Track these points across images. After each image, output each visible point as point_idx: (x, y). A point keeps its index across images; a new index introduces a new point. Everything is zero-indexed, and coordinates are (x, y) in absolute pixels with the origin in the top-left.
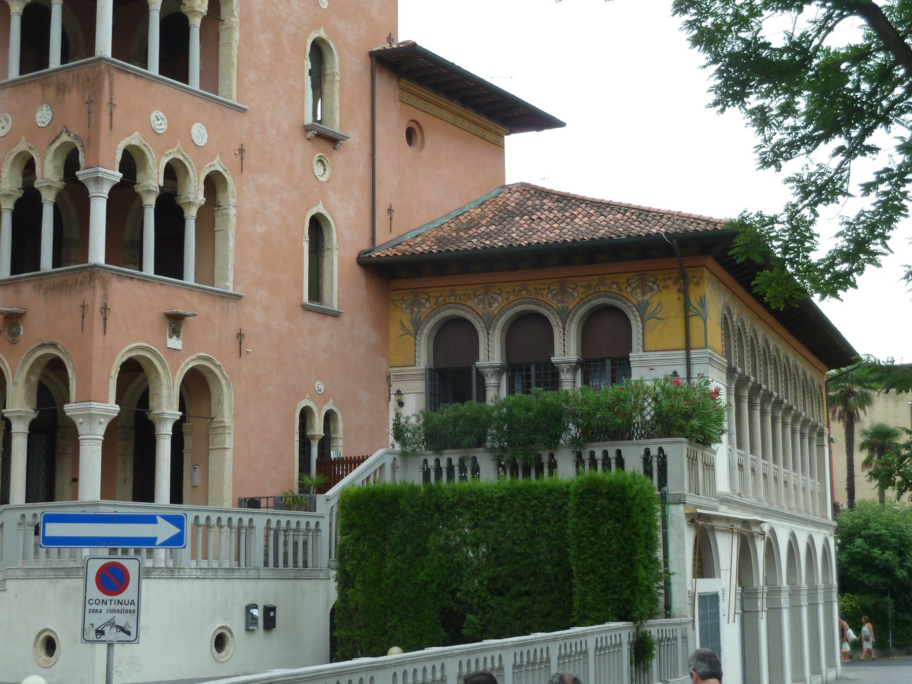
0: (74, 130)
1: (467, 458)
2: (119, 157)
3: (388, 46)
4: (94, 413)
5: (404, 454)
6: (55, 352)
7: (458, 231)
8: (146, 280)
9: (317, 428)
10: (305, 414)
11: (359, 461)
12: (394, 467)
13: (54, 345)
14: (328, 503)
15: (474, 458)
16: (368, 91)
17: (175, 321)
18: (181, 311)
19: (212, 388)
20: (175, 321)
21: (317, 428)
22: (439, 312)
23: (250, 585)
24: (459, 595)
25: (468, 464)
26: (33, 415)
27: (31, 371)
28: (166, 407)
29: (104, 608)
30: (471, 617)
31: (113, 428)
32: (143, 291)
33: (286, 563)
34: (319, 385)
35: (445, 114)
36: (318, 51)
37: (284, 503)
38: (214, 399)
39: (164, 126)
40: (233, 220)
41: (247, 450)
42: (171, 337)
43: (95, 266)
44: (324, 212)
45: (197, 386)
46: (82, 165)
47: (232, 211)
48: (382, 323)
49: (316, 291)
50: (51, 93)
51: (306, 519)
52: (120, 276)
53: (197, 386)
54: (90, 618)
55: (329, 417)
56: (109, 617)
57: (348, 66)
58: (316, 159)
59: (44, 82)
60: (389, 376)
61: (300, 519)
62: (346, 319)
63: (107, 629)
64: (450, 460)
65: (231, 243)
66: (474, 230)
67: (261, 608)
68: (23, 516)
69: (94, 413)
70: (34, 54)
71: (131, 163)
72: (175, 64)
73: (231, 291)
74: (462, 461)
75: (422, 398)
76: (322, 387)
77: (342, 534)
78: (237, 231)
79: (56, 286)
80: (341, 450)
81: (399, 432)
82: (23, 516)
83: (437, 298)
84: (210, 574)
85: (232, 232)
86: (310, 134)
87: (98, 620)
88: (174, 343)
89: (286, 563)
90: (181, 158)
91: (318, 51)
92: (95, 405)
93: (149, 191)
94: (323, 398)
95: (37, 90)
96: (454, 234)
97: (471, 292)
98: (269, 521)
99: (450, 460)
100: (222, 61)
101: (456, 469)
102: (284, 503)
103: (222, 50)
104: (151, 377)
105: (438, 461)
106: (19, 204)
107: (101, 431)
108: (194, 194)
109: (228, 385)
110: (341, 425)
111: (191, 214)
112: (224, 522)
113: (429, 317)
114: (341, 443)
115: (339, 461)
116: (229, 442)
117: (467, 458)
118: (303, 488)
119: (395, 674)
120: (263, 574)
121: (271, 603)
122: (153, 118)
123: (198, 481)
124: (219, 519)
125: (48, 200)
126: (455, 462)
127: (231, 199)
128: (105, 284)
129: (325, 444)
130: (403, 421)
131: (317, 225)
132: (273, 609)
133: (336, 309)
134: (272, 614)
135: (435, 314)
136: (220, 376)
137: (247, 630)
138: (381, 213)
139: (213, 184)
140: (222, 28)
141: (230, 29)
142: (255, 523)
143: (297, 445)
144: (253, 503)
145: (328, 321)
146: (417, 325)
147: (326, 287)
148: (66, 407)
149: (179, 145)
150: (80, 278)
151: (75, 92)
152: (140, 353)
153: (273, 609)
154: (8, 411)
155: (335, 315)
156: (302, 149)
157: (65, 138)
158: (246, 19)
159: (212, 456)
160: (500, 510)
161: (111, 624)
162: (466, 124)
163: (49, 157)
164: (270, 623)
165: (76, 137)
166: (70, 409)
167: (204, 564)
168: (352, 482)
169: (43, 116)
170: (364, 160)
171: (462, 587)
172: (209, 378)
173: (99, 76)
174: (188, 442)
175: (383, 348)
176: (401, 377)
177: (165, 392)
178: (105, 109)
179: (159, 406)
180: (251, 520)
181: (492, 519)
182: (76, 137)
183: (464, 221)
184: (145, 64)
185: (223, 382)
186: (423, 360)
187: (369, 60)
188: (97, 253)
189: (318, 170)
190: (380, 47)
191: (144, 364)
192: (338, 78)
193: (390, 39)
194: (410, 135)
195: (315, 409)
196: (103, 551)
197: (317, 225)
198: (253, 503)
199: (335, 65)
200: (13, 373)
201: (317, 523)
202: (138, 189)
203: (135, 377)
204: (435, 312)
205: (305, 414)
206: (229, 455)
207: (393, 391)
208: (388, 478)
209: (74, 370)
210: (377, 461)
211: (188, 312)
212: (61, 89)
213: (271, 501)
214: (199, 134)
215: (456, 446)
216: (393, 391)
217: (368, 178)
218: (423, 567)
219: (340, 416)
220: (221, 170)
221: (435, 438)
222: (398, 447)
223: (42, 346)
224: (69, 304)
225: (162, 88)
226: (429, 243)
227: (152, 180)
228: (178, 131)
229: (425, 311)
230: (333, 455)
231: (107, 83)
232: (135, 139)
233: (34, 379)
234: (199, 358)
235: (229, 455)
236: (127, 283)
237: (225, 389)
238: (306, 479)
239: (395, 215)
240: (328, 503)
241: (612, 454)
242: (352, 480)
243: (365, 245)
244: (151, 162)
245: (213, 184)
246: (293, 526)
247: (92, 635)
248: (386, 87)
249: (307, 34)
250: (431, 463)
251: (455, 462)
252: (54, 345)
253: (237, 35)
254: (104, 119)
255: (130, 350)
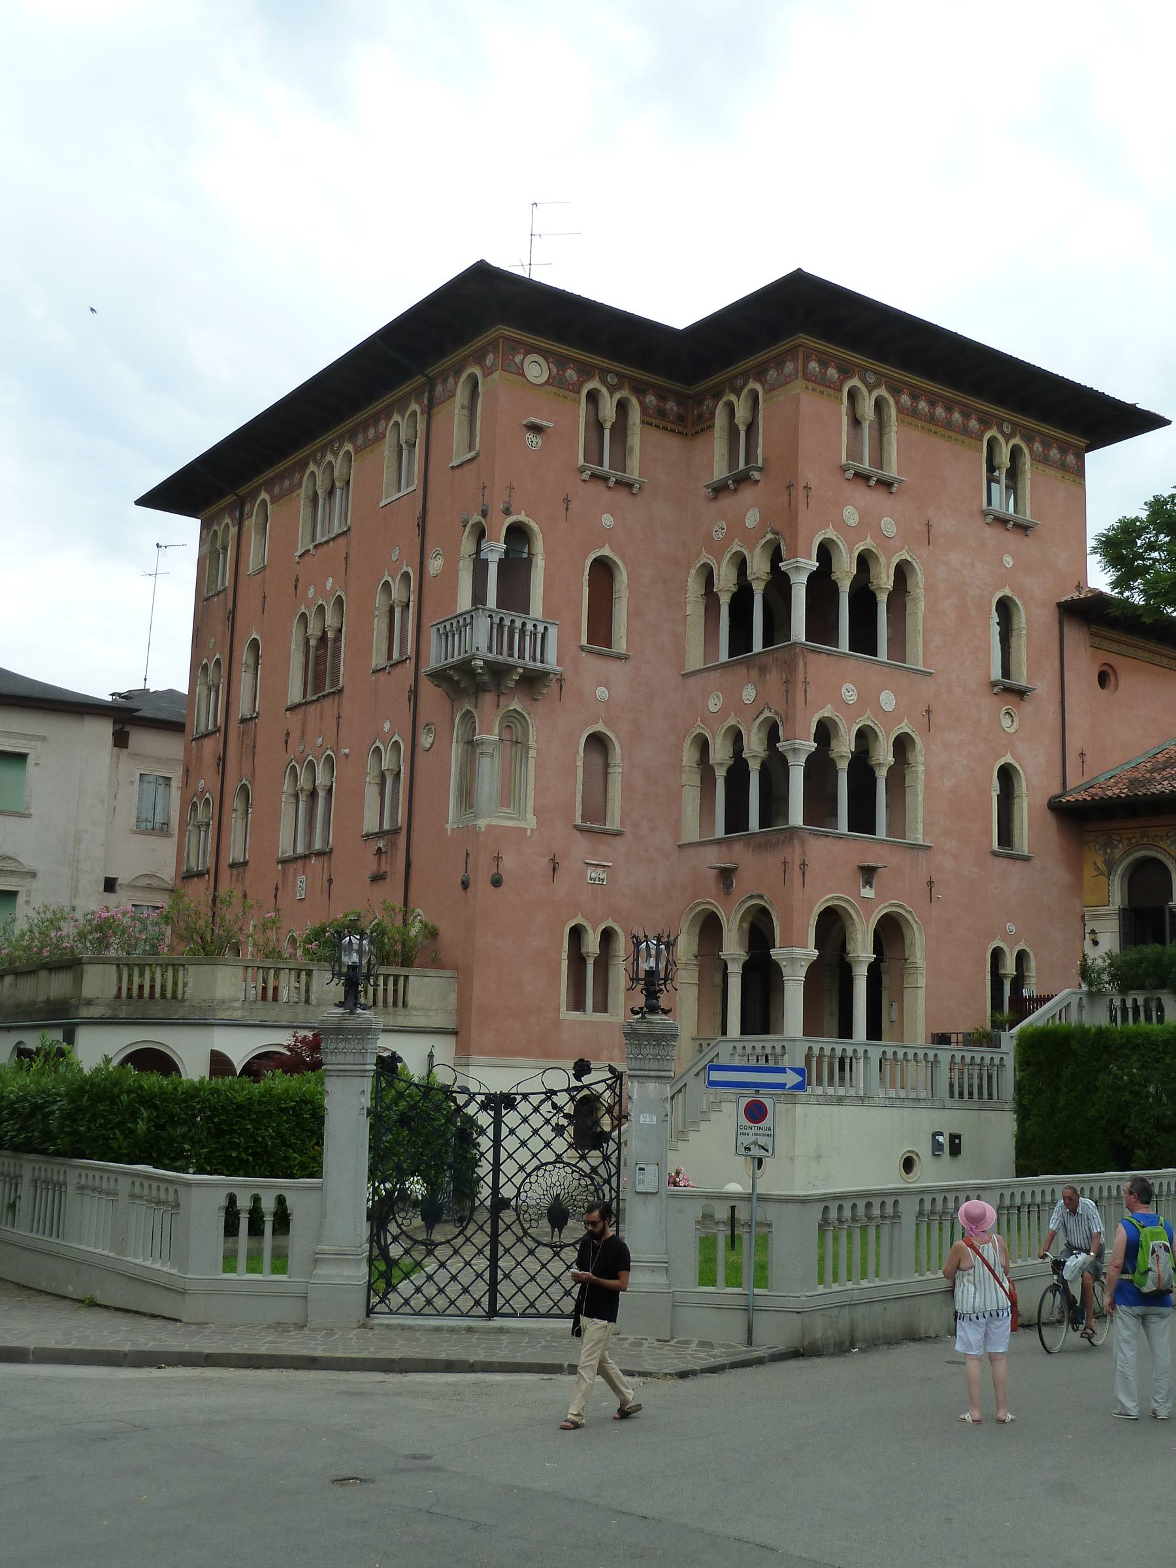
0: (774, 707)
1: (1151, 999)
2: (813, 729)
3: (1075, 596)
4: (796, 957)
5: (1090, 994)
6: (763, 903)
7: (1151, 771)
8: (840, 837)
9: (1009, 967)
10: (997, 955)
11: (1049, 999)
12: (1080, 1006)
13: (761, 897)
14: (1009, 1040)
15: (1159, 999)
16: (1057, 642)
17: (868, 873)
18: (872, 864)
19: (906, 932)
20: (868, 873)
21: (1009, 967)
22: (1132, 853)
23: (935, 1114)
24: (1127, 1131)
25: (1153, 1005)
26: (746, 958)
27: (742, 919)
28: (862, 951)
29: (750, 1132)
30: (1139, 1152)
31: (814, 971)
32: (837, 847)
33: (971, 1094)
34: (1011, 927)
35: (1141, 653)
36: (1005, 608)
37: (971, 1040)
38: (907, 942)
39: (855, 697)
40: (922, 776)
41: (939, 988)
42: (864, 887)
43: (794, 827)
44: (1012, 761)
45: (890, 932)
46: (782, 738)
47: (921, 768)
48: (1075, 866)
49: (1006, 836)
50: (754, 673)
51: (981, 1055)
52: (817, 834)
53: (890, 932)
54: (741, 1139)
55: (1021, 957)
56: (754, 1138)
57: (1035, 621)
58: (1003, 711)
59: (748, 663)
60: (1083, 916)
61: (984, 1055)
62: (1037, 863)
63: (752, 1147)
64: (1135, 1001)
65: (920, 798)
66: (1168, 770)
67: (947, 1135)
68: (735, 1048)
69: (796, 957)
70: (740, 641)
71: (825, 733)
72: (863, 641)
73: (920, 842)
74: (1146, 1001)
75: (1116, 938)
76: (1013, 928)
77: (1021, 1070)
78: (926, 787)
79: (762, 845)
80: (1034, 988)
81: (1085, 972)
82: (735, 1048)
83: (1130, 839)
84: (898, 1103)
85: (920, 787)
86: (996, 690)
87: (747, 1141)
88: (868, 892)
89: (971, 1094)
90: (871, 724)
91: (1005, 608)
92: (796, 950)
93: (842, 757)
94: (1016, 939)
95: (742, 671)
96: (1148, 775)
97: (1163, 834)
98: (953, 1056)
99: (1135, 1001)
100: (909, 629)
101: (1142, 1009)
102: (971, 1040)
103: (909, 620)
104: (848, 923)
105: (1123, 1001)
106: (730, 771)
107: (802, 973)
108: (884, 755)
109: (919, 929)
110: (1033, 964)
111: (882, 774)
112: (921, 1056)
113: (1122, 858)
114: (1033, 981)
115: (1031, 999)
116: (922, 982)
117: (1151, 999)
118: (996, 1024)
119: (1002, 1195)
120: (949, 1103)
121: (956, 1131)
122: (843, 690)
123: (894, 1017)
124: (916, 1054)
125: (754, 767)
126: (1140, 1002)
127: (918, 757)
128: (803, 843)
129: (1019, 981)
130: (1089, 962)
131: (1006, 775)
132: (959, 1137)
133: (1026, 853)
134: (957, 1141)
135: (1128, 856)
136: (911, 921)
137: (934, 1155)
138: (1072, 757)
139: (902, 745)
140: (908, 598)
141: (915, 599)
142: (939, 1058)
143: (989, 983)
144: (943, 1039)
145: (1020, 864)
146: (1111, 866)
147: (1016, 832)
148: (772, 951)
149: (868, 713)
150: (782, 838)
151: (774, 672)
152: (836, 902)
153: (959, 1137)
154: (724, 954)
155: (1026, 859)
156: (988, 703)
157: (767, 714)
158: (929, 588)
159: (907, 994)
160: (1165, 1053)
161: (755, 1143)
162: (1165, 661)
163: (755, 730)
164: (955, 1150)
165: (776, 713)
166: (774, 953)
167: (892, 1093)
168: (1031, 1024)
169: (749, 694)
170: (1054, 707)
171: (1131, 1124)
172: (902, 922)
173: (794, 659)
174: (886, 980)
175: (1077, 887)
176: (1094, 916)
177: (859, 937)
178: (800, 686)
179: (855, 950)
180: (936, 1055)
181: (1157, 1061)
182: (776, 713)
183: (1161, 760)
184: (835, 642)
185: (915, 926)
186: (1117, 899)
187: (1057, 610)
188: (796, 816)
189: (1006, 722)
190: (1067, 598)
191: (841, 912)
192: (1024, 632)
193: (1079, 588)
194: (1103, 679)
195: (1006, 949)
196: (752, 1091)
197: (1006, 775)
198: (943, 1039)
199: (1021, 620)
200: (728, 920)
201: (1002, 1059)
202: (833, 755)
203: (832, 925)
204: (1127, 853)
205: (997, 955)
206: (921, 994)
207: (1088, 930)
208: (1074, 1018)
209: (778, 918)
210: (1061, 1004)
211: (879, 865)
212: (763, 670)
213: (961, 1037)
214: (888, 700)
215: (1140, 987)
216: (1088, 930)
217: (1058, 725)
218: (1094, 1104)
219: (1032, 955)
220: (909, 731)
221: (1126, 976)
222: (1085, 988)
223: (752, 897)
224: (772, 860)
225: (852, 662)
226: (1120, 785)
227: (844, 747)
228: (868, 700)
229: (1118, 853)
230: (1025, 993)
231: (801, 664)
232: (827, 712)
233: (746, 926)
234: (892, 905)
235: (921, 994)
236: (824, 841)
237: (916, 933)
238: (998, 1016)
239: (1087, 758)
240: (1009, 1040)
241: (268, 1205)
242: (1037, 1019)
243: (1056, 790)
244: (842, 730)
245: (902, 745)
246: (968, 1060)
247: (743, 1151)
248: (1076, 637)
249: (992, 594)
250: (1117, 1002)
251: (1140, 1002)
252: (761, 897)
253: (922, 606)
254: (800, 696)
255: (827, 900)
